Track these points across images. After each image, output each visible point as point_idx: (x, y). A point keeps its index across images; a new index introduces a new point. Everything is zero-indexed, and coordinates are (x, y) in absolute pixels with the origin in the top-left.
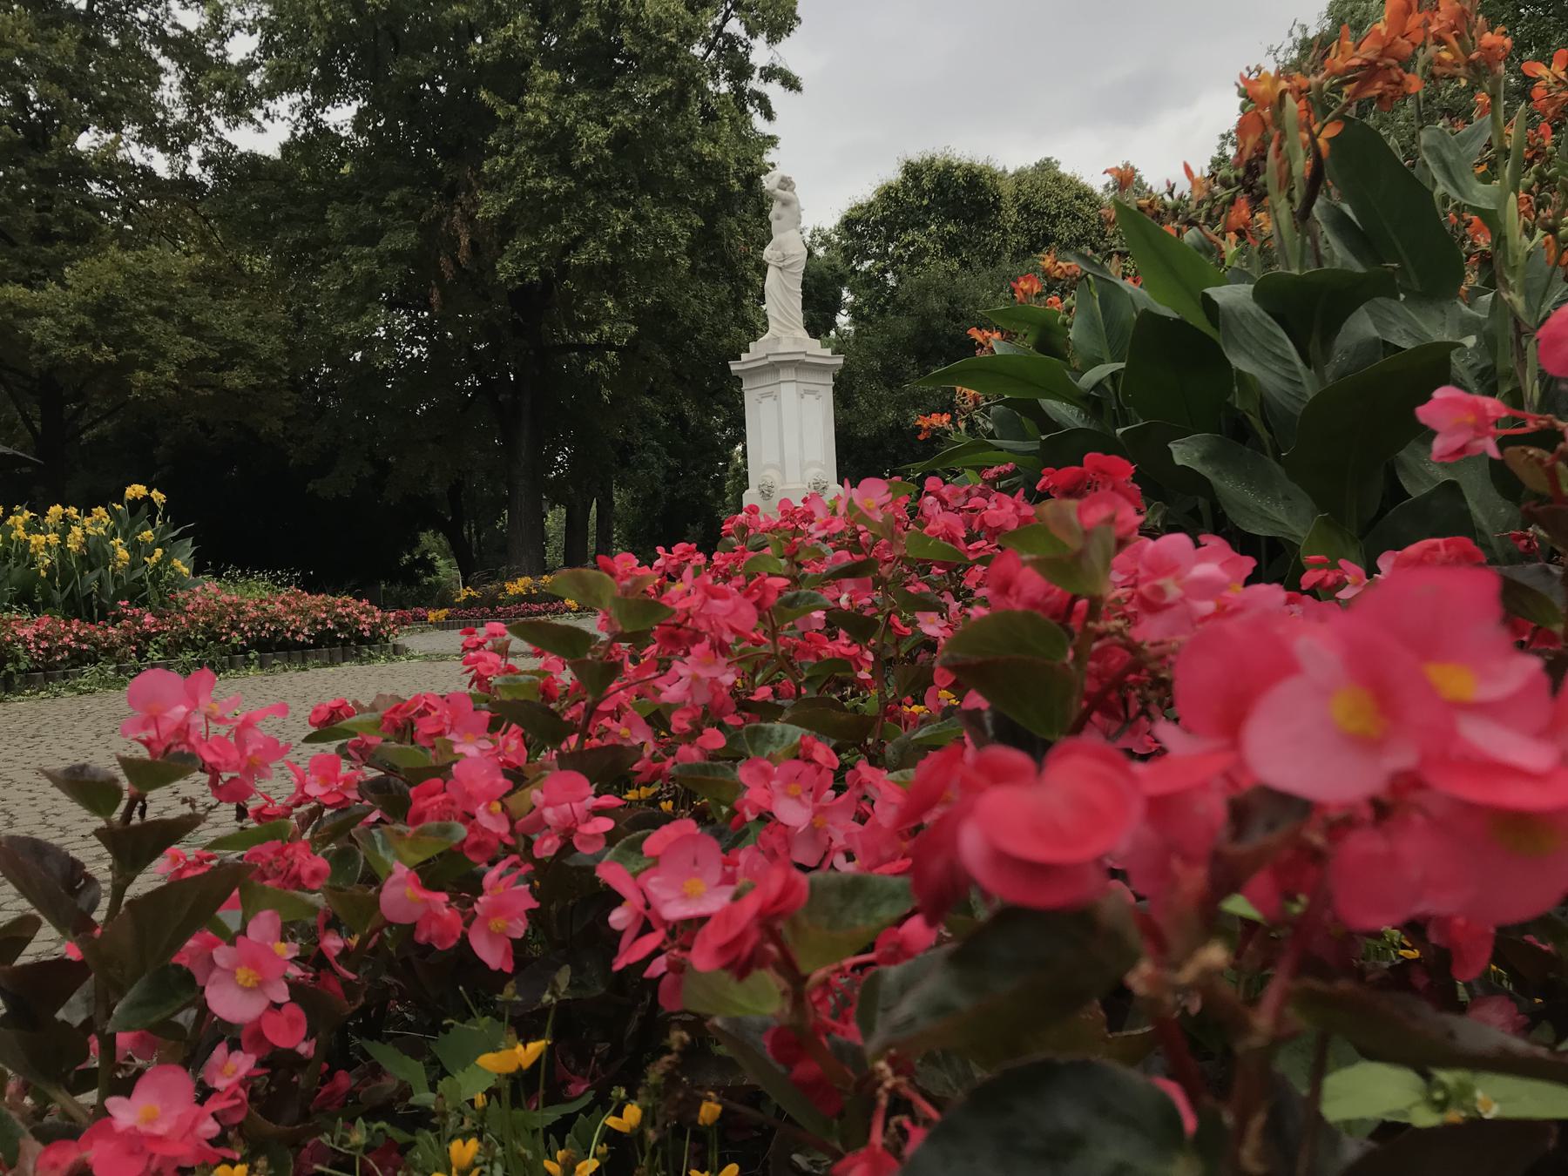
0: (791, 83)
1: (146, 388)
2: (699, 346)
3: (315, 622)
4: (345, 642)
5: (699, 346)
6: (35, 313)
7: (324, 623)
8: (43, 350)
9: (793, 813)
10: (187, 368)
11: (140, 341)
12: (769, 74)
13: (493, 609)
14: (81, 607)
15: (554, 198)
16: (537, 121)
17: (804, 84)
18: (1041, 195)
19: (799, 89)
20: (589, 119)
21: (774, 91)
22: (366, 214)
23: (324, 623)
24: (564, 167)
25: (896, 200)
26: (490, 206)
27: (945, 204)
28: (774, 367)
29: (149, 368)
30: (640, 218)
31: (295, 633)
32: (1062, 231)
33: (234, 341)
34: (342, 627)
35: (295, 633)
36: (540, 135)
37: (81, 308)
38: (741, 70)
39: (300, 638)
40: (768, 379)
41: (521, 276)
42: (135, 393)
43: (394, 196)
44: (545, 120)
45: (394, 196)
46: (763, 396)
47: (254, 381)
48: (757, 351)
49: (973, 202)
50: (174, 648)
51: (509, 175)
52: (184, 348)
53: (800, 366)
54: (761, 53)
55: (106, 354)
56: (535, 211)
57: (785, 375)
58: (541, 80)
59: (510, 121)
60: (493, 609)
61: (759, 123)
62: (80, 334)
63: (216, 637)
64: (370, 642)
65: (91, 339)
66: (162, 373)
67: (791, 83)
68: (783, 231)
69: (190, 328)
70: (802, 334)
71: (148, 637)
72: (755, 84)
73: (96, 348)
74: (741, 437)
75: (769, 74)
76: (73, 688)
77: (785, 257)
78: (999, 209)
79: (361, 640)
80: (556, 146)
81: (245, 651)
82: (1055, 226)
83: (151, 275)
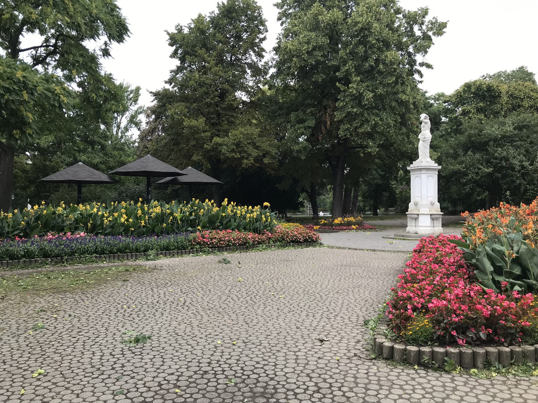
0: (429, 66)
1: (246, 164)
2: (394, 149)
3: (304, 236)
4: (310, 242)
5: (394, 149)
6: (221, 145)
7: (306, 237)
8: (223, 154)
9: (435, 302)
10: (256, 159)
11: (245, 152)
12: (422, 65)
13: (332, 227)
14: (256, 231)
15: (356, 114)
16: (352, 92)
17: (433, 67)
18: (517, 91)
19: (432, 68)
20: (368, 90)
21: (423, 70)
22: (301, 114)
23: (306, 237)
24: (360, 104)
25: (461, 96)
26: (339, 115)
27: (481, 96)
28: (420, 169)
29: (247, 158)
30: (381, 119)
31: (300, 239)
32: (526, 104)
33: (266, 151)
34: (310, 238)
35: (300, 239)
36: (353, 95)
37: (233, 144)
38: (412, 63)
39: (301, 240)
40: (418, 172)
41: (345, 136)
42: (243, 166)
43: (309, 111)
44: (355, 92)
45: (309, 111)
46: (417, 177)
47: (270, 162)
48: (416, 164)
49: (490, 95)
50: (275, 241)
51: (343, 107)
52: (255, 153)
53: (428, 169)
54: (419, 58)
55: (238, 156)
56: (350, 117)
57: (423, 172)
58: (354, 79)
59: (344, 91)
60: (332, 227)
61: (416, 76)
62: (233, 151)
63: (284, 239)
64: (315, 242)
65: (235, 152)
66: (250, 160)
67: (429, 66)
68: (424, 131)
69: (257, 148)
70: (429, 159)
71: (270, 238)
72: (417, 67)
73: (236, 154)
74: (410, 190)
75: (422, 65)
76: (258, 250)
77: (425, 138)
78: (500, 97)
79: (313, 241)
80: (358, 99)
81: (290, 243)
82: (523, 102)
83: (248, 134)
